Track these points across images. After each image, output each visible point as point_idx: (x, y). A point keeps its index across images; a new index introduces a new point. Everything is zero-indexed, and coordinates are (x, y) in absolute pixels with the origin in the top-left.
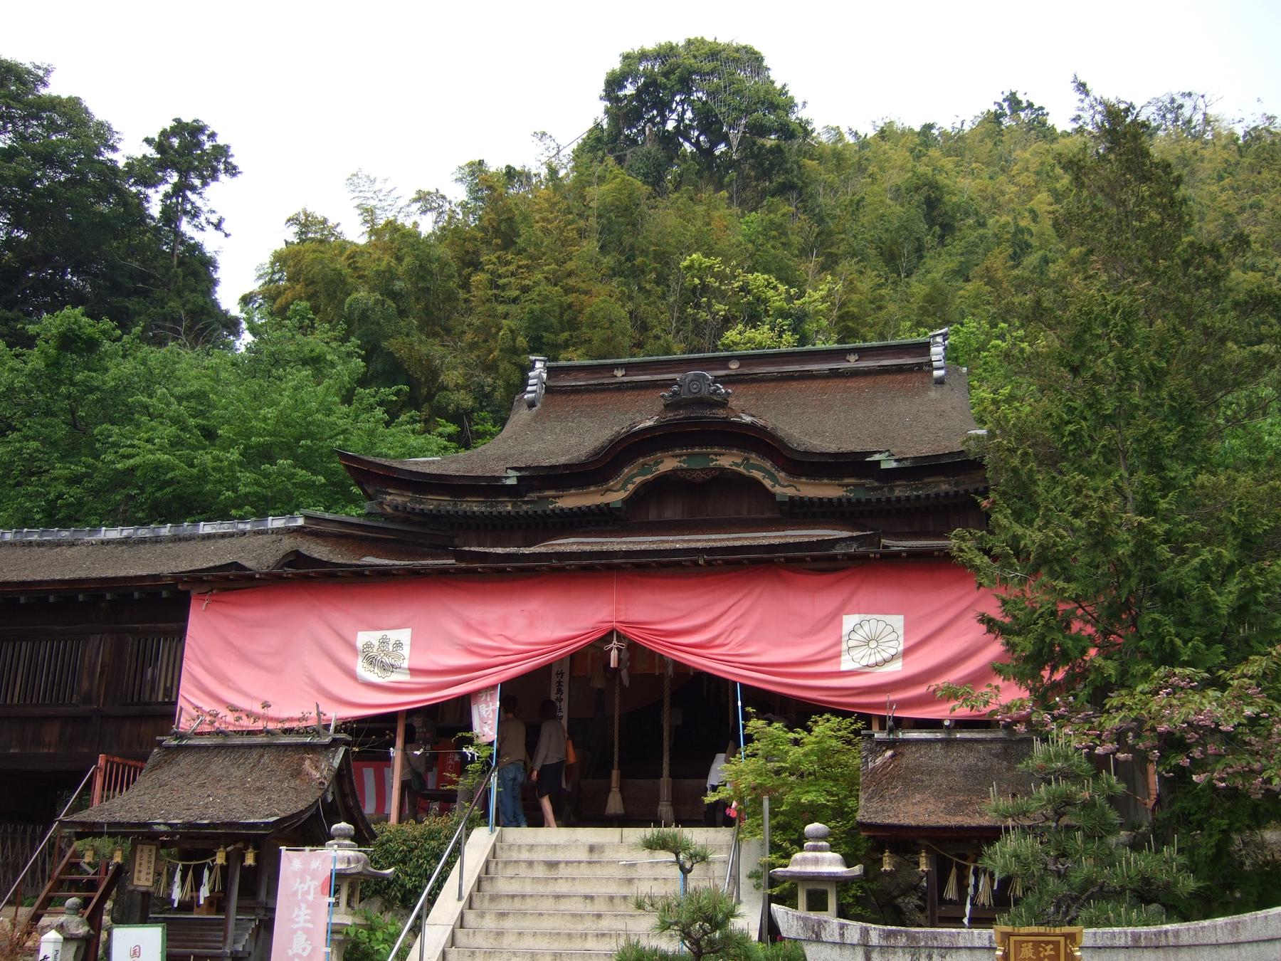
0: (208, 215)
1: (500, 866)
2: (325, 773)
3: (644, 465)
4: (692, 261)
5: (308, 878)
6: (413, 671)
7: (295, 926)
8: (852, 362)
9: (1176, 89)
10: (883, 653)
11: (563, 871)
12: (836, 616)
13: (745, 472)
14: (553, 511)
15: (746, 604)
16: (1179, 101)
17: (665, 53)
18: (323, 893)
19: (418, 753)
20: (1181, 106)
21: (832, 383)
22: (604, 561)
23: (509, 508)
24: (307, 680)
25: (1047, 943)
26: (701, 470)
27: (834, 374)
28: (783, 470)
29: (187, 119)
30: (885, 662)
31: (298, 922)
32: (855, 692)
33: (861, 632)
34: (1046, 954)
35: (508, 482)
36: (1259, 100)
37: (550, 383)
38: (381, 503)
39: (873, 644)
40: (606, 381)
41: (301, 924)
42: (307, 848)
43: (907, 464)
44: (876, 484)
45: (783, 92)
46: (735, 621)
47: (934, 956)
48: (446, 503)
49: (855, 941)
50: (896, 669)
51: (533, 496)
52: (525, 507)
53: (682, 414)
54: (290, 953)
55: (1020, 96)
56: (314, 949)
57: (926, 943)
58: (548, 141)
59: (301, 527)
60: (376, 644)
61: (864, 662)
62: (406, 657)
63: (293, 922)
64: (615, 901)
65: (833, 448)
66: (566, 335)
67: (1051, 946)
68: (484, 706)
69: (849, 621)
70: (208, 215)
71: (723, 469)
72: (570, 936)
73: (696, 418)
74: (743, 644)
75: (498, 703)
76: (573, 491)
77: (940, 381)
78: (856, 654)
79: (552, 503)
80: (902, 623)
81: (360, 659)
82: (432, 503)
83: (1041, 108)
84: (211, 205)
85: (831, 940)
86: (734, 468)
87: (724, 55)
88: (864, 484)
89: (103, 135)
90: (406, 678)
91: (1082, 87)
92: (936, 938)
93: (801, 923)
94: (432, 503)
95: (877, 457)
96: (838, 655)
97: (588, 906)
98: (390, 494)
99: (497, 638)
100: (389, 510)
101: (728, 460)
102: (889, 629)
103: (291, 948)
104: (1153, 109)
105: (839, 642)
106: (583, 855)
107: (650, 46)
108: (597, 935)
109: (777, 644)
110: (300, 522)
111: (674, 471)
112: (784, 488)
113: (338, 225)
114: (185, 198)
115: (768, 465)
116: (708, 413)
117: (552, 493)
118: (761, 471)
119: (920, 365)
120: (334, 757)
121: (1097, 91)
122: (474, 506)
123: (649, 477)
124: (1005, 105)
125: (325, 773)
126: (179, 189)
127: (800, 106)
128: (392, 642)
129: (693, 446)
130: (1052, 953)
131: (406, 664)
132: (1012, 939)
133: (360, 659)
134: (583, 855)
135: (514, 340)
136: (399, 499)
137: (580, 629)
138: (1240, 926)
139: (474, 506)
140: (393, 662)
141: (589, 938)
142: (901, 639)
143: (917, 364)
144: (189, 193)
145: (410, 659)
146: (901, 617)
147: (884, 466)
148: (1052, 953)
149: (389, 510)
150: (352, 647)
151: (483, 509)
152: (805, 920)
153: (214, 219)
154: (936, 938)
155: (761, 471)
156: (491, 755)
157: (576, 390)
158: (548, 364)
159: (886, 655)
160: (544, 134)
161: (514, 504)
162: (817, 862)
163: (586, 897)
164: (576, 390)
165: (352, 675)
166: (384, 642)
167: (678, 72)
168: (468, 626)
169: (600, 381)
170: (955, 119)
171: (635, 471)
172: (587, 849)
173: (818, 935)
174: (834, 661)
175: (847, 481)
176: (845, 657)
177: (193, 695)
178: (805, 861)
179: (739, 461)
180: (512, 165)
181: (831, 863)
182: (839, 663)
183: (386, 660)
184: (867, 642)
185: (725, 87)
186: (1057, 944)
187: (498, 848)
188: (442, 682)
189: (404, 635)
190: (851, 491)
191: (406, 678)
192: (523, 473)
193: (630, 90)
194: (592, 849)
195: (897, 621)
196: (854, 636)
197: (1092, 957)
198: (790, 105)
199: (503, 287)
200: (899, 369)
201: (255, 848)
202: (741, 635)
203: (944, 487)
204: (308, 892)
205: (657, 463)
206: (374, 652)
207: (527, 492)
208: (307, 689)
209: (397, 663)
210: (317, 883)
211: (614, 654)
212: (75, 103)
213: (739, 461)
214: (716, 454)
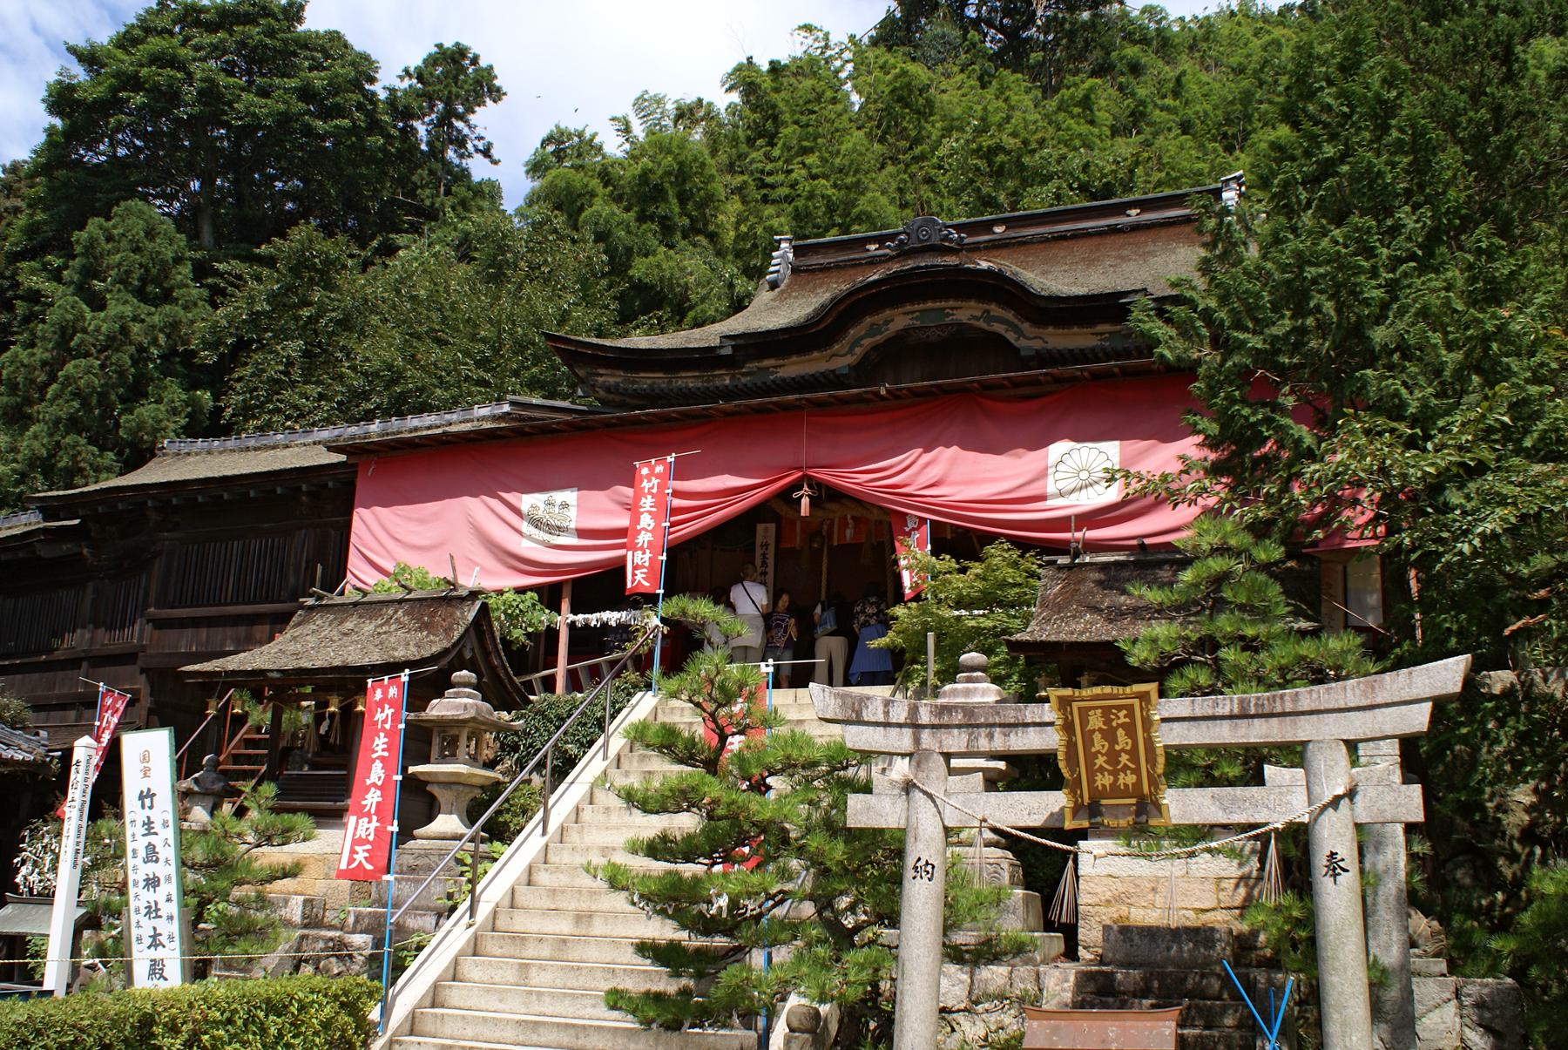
0: (476, 142)
5: (387, 706)
6: (581, 533)
14: (774, 382)
21: (1109, 240)
22: (775, 399)
23: (727, 382)
25: (1119, 708)
26: (937, 327)
27: (1114, 230)
28: (1028, 320)
29: (449, 44)
34: (1120, 722)
38: (593, 386)
40: (857, 256)
41: (380, 753)
47: (996, 735)
49: (902, 720)
51: (751, 366)
52: (744, 380)
54: (368, 782)
57: (986, 719)
59: (508, 414)
67: (1124, 712)
70: (476, 142)
71: (961, 325)
73: (926, 267)
76: (794, 358)
79: (773, 373)
82: (647, 380)
84: (479, 131)
85: (873, 719)
89: (364, 69)
92: (998, 713)
93: (839, 701)
94: (647, 380)
98: (602, 375)
101: (966, 312)
110: (506, 408)
111: (906, 330)
112: (1031, 339)
113: (596, 134)
114: (451, 125)
115: (1010, 315)
118: (998, 320)
122: (688, 380)
126: (445, 120)
129: (925, 300)
130: (1127, 720)
132: (1075, 705)
138: (1376, 685)
139: (688, 380)
144: (454, 120)
148: (1127, 720)
152: (843, 697)
153: (480, 145)
154: (998, 713)
155: (998, 320)
157: (824, 269)
161: (733, 377)
162: (967, 693)
173: (859, 713)
177: (363, 572)
178: (954, 693)
186: (1130, 708)
187: (659, 711)
189: (570, 496)
190: (1106, 340)
192: (741, 342)
196: (1061, 467)
197: (1189, 730)
199: (773, 186)
205: (887, 322)
207: (745, 362)
211: (805, 502)
212: (335, 37)
213: (978, 314)
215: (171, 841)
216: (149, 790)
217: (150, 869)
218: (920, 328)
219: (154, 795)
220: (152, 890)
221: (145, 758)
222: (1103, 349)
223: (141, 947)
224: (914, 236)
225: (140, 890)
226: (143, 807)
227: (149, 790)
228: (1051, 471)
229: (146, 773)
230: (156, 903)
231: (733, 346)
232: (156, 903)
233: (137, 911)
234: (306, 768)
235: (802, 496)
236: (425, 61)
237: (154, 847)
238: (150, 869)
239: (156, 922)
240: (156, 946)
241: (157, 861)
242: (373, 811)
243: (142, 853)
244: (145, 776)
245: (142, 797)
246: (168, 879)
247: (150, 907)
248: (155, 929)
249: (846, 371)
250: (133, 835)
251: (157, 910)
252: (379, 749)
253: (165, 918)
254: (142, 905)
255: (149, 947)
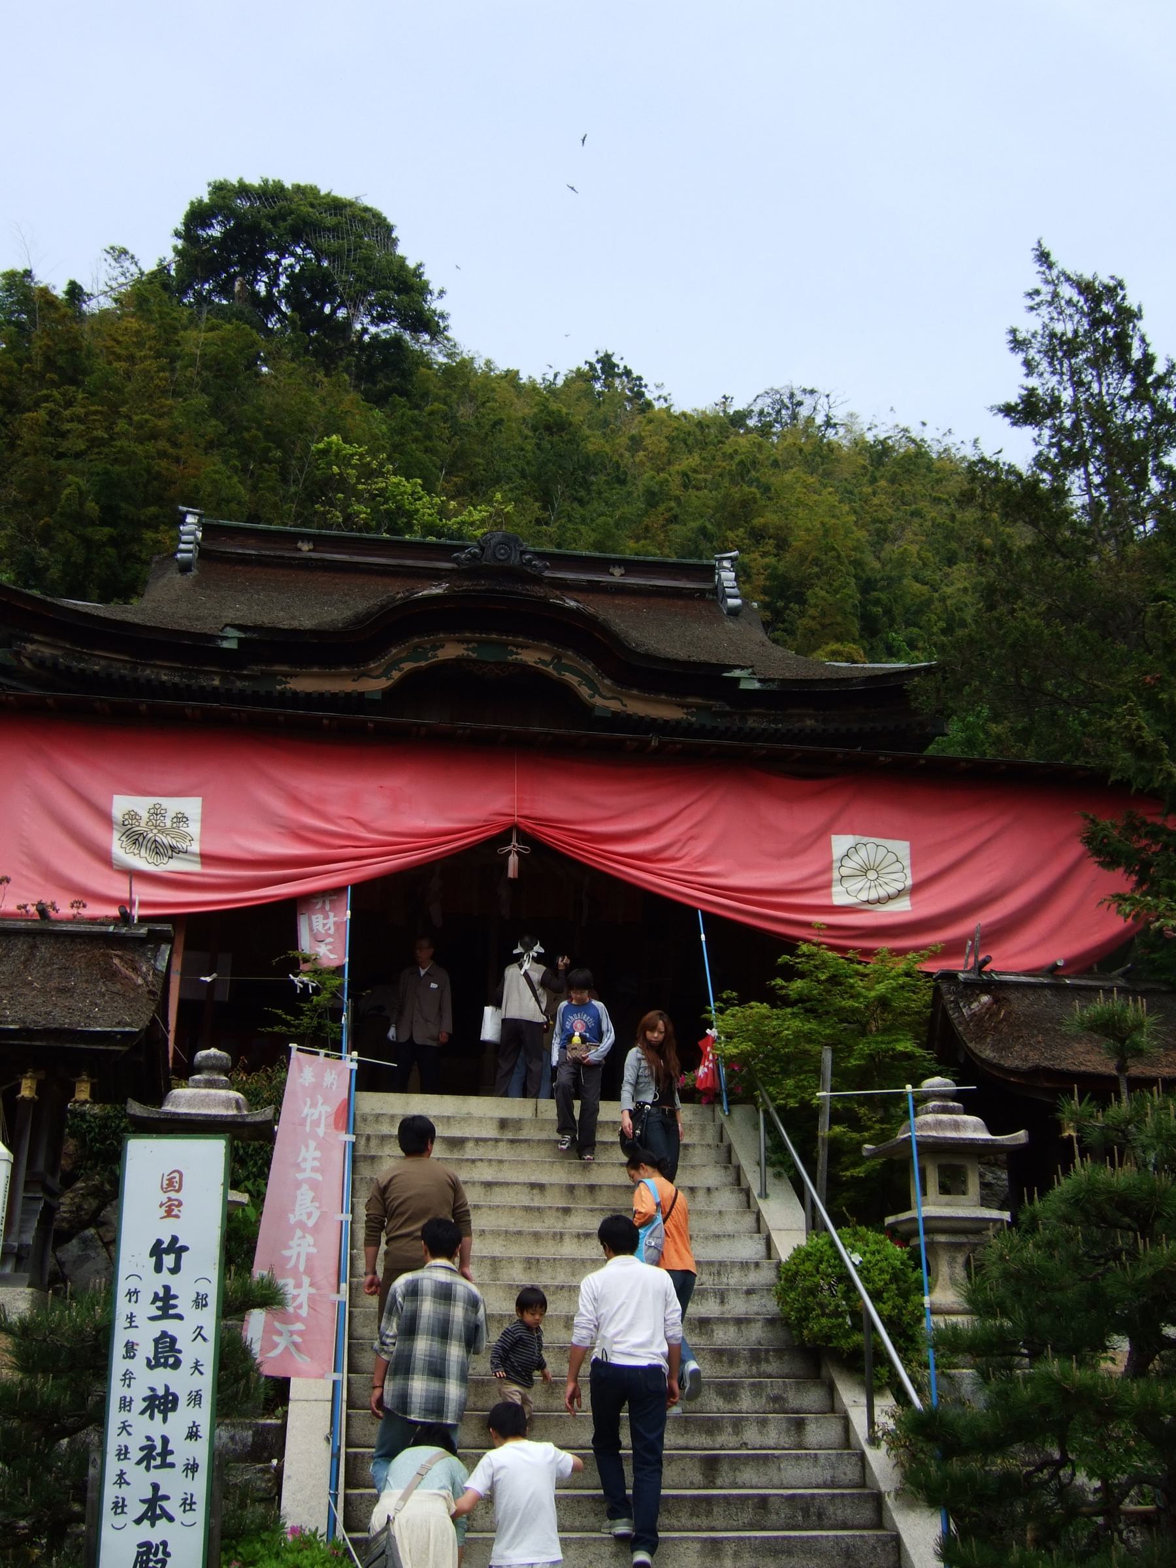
1: (373, 1142)
2: (150, 978)
3: (418, 646)
4: (330, 443)
6: (207, 859)
7: (300, 1176)
8: (617, 576)
9: (800, 381)
10: (886, 887)
11: (470, 1152)
12: (821, 836)
13: (555, 673)
15: (700, 810)
16: (799, 397)
17: (271, 194)
18: (337, 1127)
19: (208, 979)
20: (800, 404)
23: (216, 682)
24: (25, 859)
28: (609, 677)
30: (890, 898)
31: (304, 1170)
32: (858, 932)
33: (856, 858)
35: (226, 645)
36: (892, 409)
37: (205, 545)
39: (872, 875)
40: (287, 554)
41: (308, 1174)
42: (323, 1052)
43: (773, 687)
44: (728, 708)
45: (417, 273)
46: (691, 828)
48: (119, 665)
50: (903, 908)
51: (256, 669)
53: (484, 584)
55: (615, 360)
56: (323, 1216)
58: (127, 264)
60: (145, 815)
61: (863, 896)
62: (194, 836)
63: (297, 1166)
64: (577, 1192)
65: (682, 655)
66: (153, 510)
68: (320, 916)
69: (840, 843)
71: (524, 667)
72: (536, 1236)
74: (702, 860)
75: (349, 912)
77: (734, 612)
78: (855, 885)
80: (908, 851)
81: (116, 835)
82: (98, 663)
83: (640, 378)
86: (540, 666)
87: (348, 211)
88: (710, 707)
90: (196, 868)
91: (1044, 257)
95: (737, 673)
96: (828, 885)
97: (537, 1198)
98: (33, 642)
99: (344, 822)
100: (28, 664)
102: (893, 858)
103: (293, 1211)
104: (769, 401)
105: (828, 869)
106: (491, 1132)
107: (254, 181)
108: (578, 1236)
109: (747, 866)
111: (458, 660)
116: (519, 588)
117: (285, 668)
119: (702, 592)
120: (155, 958)
121: (1065, 261)
123: (423, 664)
124: (598, 366)
125: (150, 978)
127: (436, 294)
128: (171, 814)
131: (195, 848)
133: (116, 835)
134: (491, 1132)
135: (81, 505)
136: (47, 651)
137: (461, 821)
140: (173, 843)
141: (567, 1239)
142: (908, 871)
143: (698, 590)
145: (201, 841)
146: (906, 844)
147: (744, 685)
149: (28, 664)
150: (106, 818)
151: (177, 679)
156: (342, 985)
158: (204, 521)
159: (891, 890)
160: (124, 252)
162: (956, 1126)
163: (533, 1186)
164: (244, 560)
165: (104, 858)
166: (156, 812)
167: (290, 220)
168: (296, 801)
169: (278, 553)
170: (547, 370)
171: (404, 655)
172: (495, 1125)
174: (825, 892)
175: (690, 700)
176: (836, 889)
179: (547, 658)
180: (79, 282)
181: (975, 1129)
182: (830, 896)
183: (162, 838)
184: (864, 871)
185: (349, 250)
188: (255, 877)
189: (192, 806)
190: (692, 714)
191: (196, 868)
192: (248, 635)
193: (216, 232)
194: (503, 1124)
195: (902, 848)
196: (847, 862)
198: (423, 289)
199: (63, 435)
200: (677, 593)
201: (91, 1076)
202: (699, 848)
203: (809, 723)
204: (316, 1123)
205: (436, 647)
206: (142, 827)
208: (25, 872)
209: (183, 845)
210: (329, 1109)
211: (513, 860)
213: (547, 658)
214: (517, 646)
215: (210, 1332)
216: (175, 1239)
217: (161, 1379)
218: (474, 661)
219: (185, 1249)
220: (158, 1416)
221: (173, 1182)
222: (691, 724)
223: (120, 1520)
224: (489, 552)
225: (134, 1417)
226: (158, 1268)
227: (175, 1239)
228: (836, 865)
229: (171, 1210)
230: (165, 1440)
231: (240, 640)
232: (165, 1440)
233: (123, 1453)
234: (857, 1258)
235: (510, 852)
236: (298, 188)
237: (173, 1340)
238: (161, 1379)
239: (157, 1475)
240: (153, 1520)
241: (177, 1364)
242: (302, 1268)
243: (146, 1350)
244: (169, 1213)
245: (158, 1251)
246: (195, 1398)
247: (153, 1447)
248: (156, 1487)
249: (378, 697)
250: (131, 1318)
251: (166, 1452)
252: (307, 1165)
253: (180, 1467)
254: (135, 1444)
255: (138, 1521)
